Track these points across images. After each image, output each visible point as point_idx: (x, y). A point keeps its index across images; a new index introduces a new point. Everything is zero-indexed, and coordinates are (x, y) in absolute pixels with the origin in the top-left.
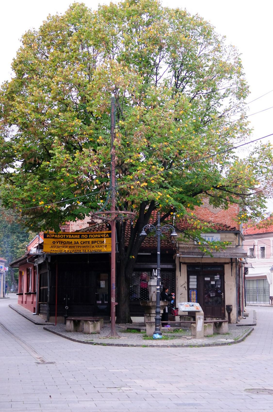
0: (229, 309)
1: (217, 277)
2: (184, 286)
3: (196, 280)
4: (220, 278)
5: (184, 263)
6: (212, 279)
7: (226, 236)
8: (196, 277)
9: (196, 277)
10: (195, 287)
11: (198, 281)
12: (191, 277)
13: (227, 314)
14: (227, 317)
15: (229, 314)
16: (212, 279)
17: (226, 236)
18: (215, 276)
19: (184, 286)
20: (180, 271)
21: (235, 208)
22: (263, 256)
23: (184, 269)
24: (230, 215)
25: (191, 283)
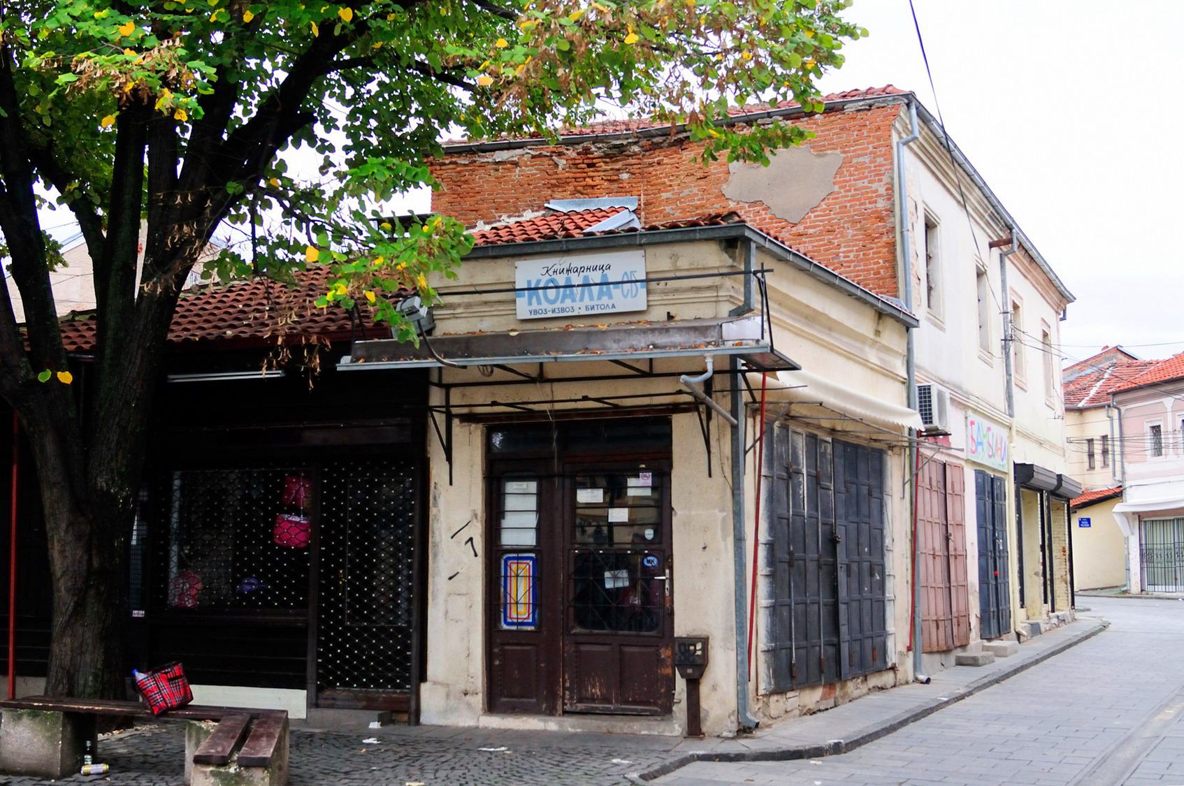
0: (693, 660)
1: (640, 486)
2: (464, 535)
3: (531, 503)
4: (654, 488)
5: (469, 418)
6: (616, 495)
7: (674, 257)
8: (532, 486)
9: (532, 486)
10: (529, 539)
11: (543, 509)
12: (511, 487)
13: (681, 684)
14: (684, 704)
15: (694, 684)
16: (616, 495)
17: (674, 257)
18: (631, 482)
19: (464, 535)
20: (449, 459)
21: (875, 186)
22: (1158, 451)
23: (469, 448)
24: (854, 222)
25: (509, 521)
